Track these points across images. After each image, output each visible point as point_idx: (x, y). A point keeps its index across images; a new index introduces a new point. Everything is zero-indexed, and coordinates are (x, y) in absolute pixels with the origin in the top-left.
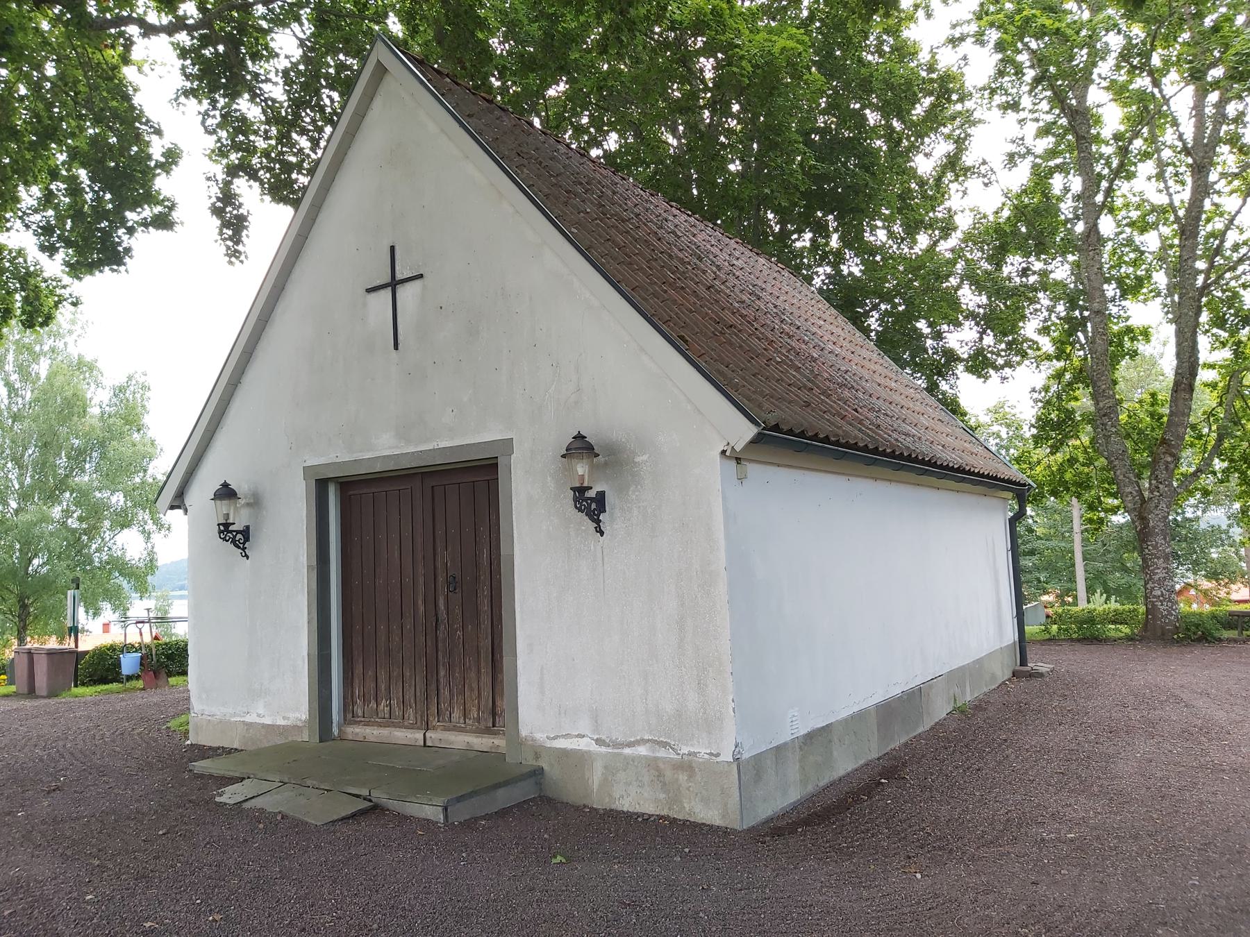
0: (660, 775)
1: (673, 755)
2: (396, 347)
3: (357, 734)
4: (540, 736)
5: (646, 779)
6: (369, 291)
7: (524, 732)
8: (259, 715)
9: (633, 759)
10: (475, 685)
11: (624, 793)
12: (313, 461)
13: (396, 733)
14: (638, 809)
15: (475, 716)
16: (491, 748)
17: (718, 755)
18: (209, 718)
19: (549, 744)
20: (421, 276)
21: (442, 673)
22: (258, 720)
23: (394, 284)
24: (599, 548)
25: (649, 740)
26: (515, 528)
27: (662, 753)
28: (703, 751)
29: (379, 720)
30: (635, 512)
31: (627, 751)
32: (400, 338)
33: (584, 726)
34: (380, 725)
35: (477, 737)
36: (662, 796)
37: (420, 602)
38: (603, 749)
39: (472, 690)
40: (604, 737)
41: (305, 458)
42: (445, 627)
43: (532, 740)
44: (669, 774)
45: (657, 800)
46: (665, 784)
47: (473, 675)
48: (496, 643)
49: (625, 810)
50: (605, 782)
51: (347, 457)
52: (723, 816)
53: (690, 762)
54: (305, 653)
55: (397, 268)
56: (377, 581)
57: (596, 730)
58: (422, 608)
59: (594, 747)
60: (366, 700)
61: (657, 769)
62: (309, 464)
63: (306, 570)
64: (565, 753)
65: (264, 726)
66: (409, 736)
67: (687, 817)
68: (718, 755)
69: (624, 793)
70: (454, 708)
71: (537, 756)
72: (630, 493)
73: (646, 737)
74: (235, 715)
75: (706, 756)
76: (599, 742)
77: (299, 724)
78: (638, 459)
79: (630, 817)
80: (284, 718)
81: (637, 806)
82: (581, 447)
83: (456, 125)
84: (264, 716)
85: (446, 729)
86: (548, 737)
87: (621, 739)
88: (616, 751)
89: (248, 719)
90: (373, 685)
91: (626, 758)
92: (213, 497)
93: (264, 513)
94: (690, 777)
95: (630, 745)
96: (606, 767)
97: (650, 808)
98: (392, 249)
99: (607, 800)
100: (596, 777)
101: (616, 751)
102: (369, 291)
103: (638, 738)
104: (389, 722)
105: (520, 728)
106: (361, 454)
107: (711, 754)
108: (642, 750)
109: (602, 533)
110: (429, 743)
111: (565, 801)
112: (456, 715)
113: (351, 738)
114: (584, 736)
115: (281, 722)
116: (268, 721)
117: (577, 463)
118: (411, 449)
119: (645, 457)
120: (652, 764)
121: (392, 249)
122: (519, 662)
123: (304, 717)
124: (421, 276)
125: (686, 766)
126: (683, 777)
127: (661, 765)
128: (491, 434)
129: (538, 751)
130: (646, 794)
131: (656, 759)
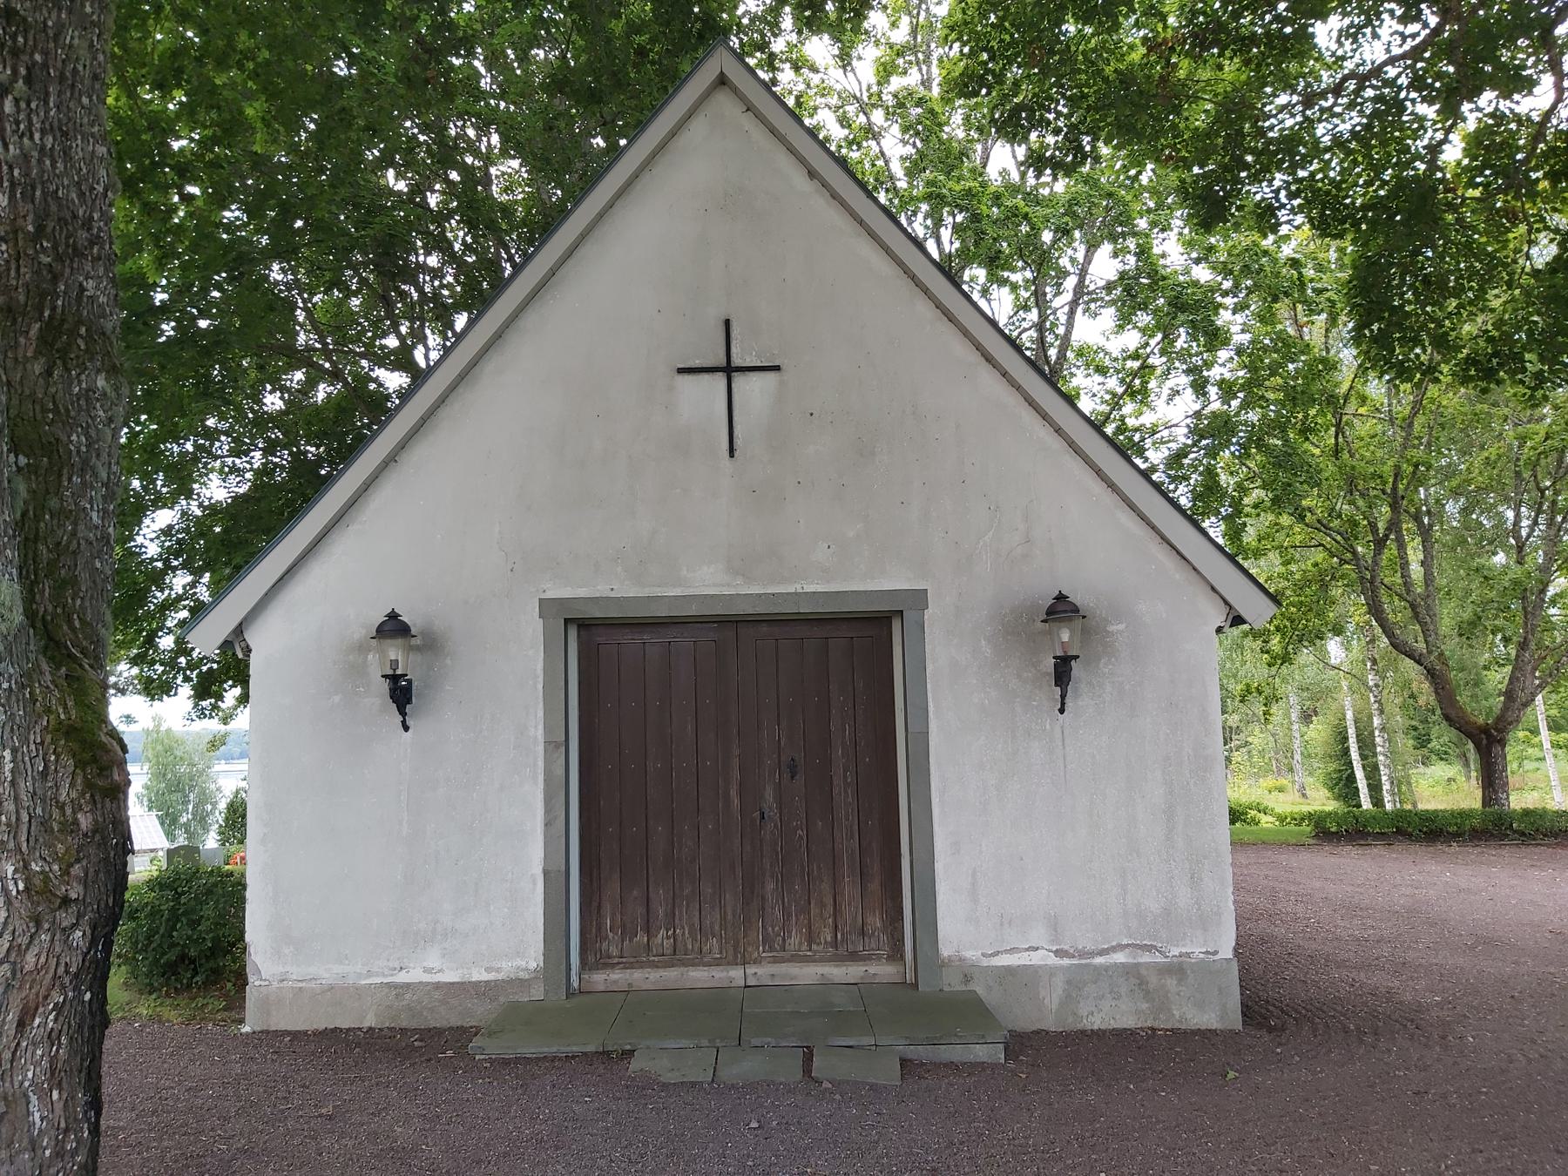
0: (1142, 983)
1: (1159, 959)
3: (615, 982)
4: (971, 954)
5: (1123, 990)
6: (681, 371)
7: (946, 951)
8: (427, 970)
9: (1106, 968)
10: (829, 900)
11: (1094, 1009)
13: (691, 974)
14: (1114, 1025)
15: (829, 939)
16: (862, 978)
17: (1216, 953)
18: (300, 985)
19: (985, 962)
20: (777, 368)
22: (427, 978)
23: (729, 370)
24: (1058, 731)
25: (1128, 945)
26: (930, 700)
27: (1146, 958)
28: (1197, 950)
29: (656, 959)
30: (1108, 688)
31: (1099, 960)
32: (738, 442)
33: (1038, 935)
34: (655, 965)
36: (1145, 1006)
37: (733, 793)
38: (1066, 962)
39: (822, 905)
40: (1066, 947)
42: (776, 826)
43: (960, 960)
44: (1153, 980)
45: (1138, 1012)
46: (1148, 992)
47: (826, 886)
49: (1096, 1027)
50: (1068, 1000)
52: (1222, 1018)
53: (1181, 963)
54: (537, 869)
55: (734, 350)
57: (1052, 942)
58: (736, 801)
59: (1053, 960)
60: (627, 932)
61: (1139, 976)
62: (550, 595)
64: (1010, 971)
65: (438, 986)
66: (723, 974)
67: (1177, 1025)
68: (1216, 953)
69: (1094, 1009)
70: (790, 932)
71: (967, 979)
72: (1101, 665)
73: (1125, 942)
74: (369, 974)
75: (1202, 956)
76: (1059, 953)
78: (1111, 628)
79: (1099, 1034)
80: (488, 970)
81: (1112, 1022)
82: (393, 627)
85: (775, 960)
86: (983, 955)
87: (1090, 947)
88: (1083, 962)
89: (402, 978)
90: (641, 910)
91: (1096, 968)
92: (374, 634)
93: (448, 662)
94: (1180, 981)
95: (1102, 952)
96: (1069, 982)
97: (1128, 1021)
98: (727, 323)
99: (1070, 1020)
100: (1052, 997)
101: (1083, 962)
102: (681, 371)
103: (1114, 944)
104: (676, 957)
105: (940, 946)
107: (1207, 953)
108: (1120, 958)
109: (406, 728)
110: (750, 983)
112: (794, 941)
113: (602, 988)
114: (1037, 949)
117: (1060, 628)
119: (1121, 627)
120: (1130, 971)
121: (727, 323)
122: (939, 866)
123: (533, 965)
124: (777, 368)
125: (1177, 969)
126: (1171, 983)
127: (1144, 972)
128: (892, 580)
129: (968, 973)
130: (1124, 1007)
131: (1138, 965)
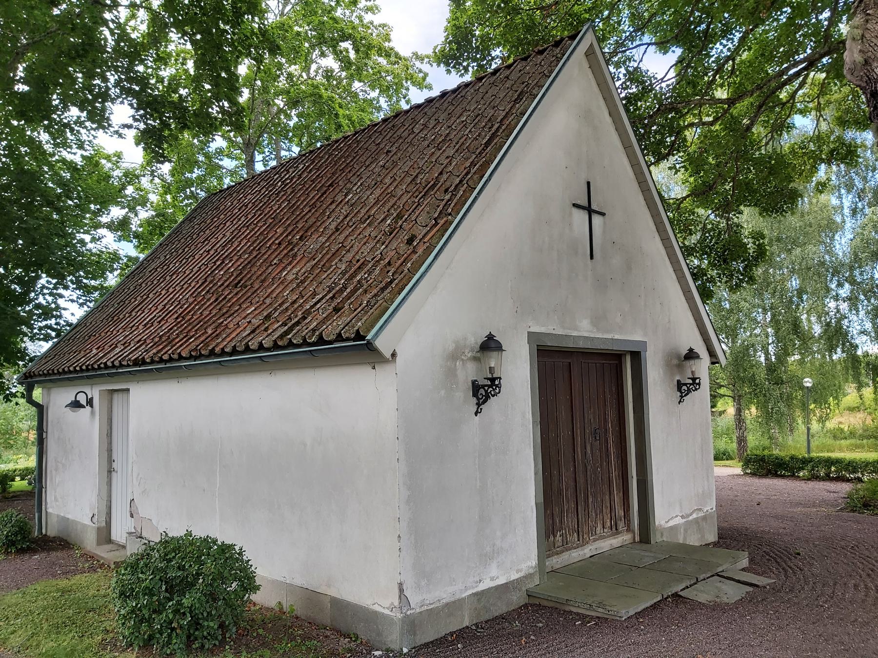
2: (592, 257)
8: (492, 579)
12: (535, 329)
21: (590, 500)
35: (615, 538)
41: (530, 324)
48: (105, 488)
51: (560, 331)
56: (550, 434)
62: (532, 330)
63: (531, 426)
66: (581, 553)
74: (466, 589)
77: (531, 571)
80: (518, 571)
83: (558, 79)
84: (498, 577)
89: (482, 587)
98: (588, 183)
106: (569, 331)
108: (695, 516)
111: (363, 637)
115: (514, 576)
116: (502, 581)
118: (600, 336)
